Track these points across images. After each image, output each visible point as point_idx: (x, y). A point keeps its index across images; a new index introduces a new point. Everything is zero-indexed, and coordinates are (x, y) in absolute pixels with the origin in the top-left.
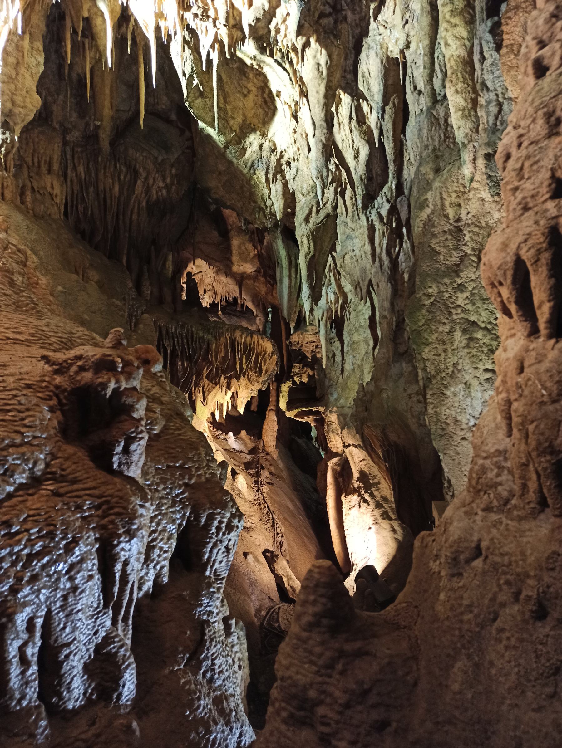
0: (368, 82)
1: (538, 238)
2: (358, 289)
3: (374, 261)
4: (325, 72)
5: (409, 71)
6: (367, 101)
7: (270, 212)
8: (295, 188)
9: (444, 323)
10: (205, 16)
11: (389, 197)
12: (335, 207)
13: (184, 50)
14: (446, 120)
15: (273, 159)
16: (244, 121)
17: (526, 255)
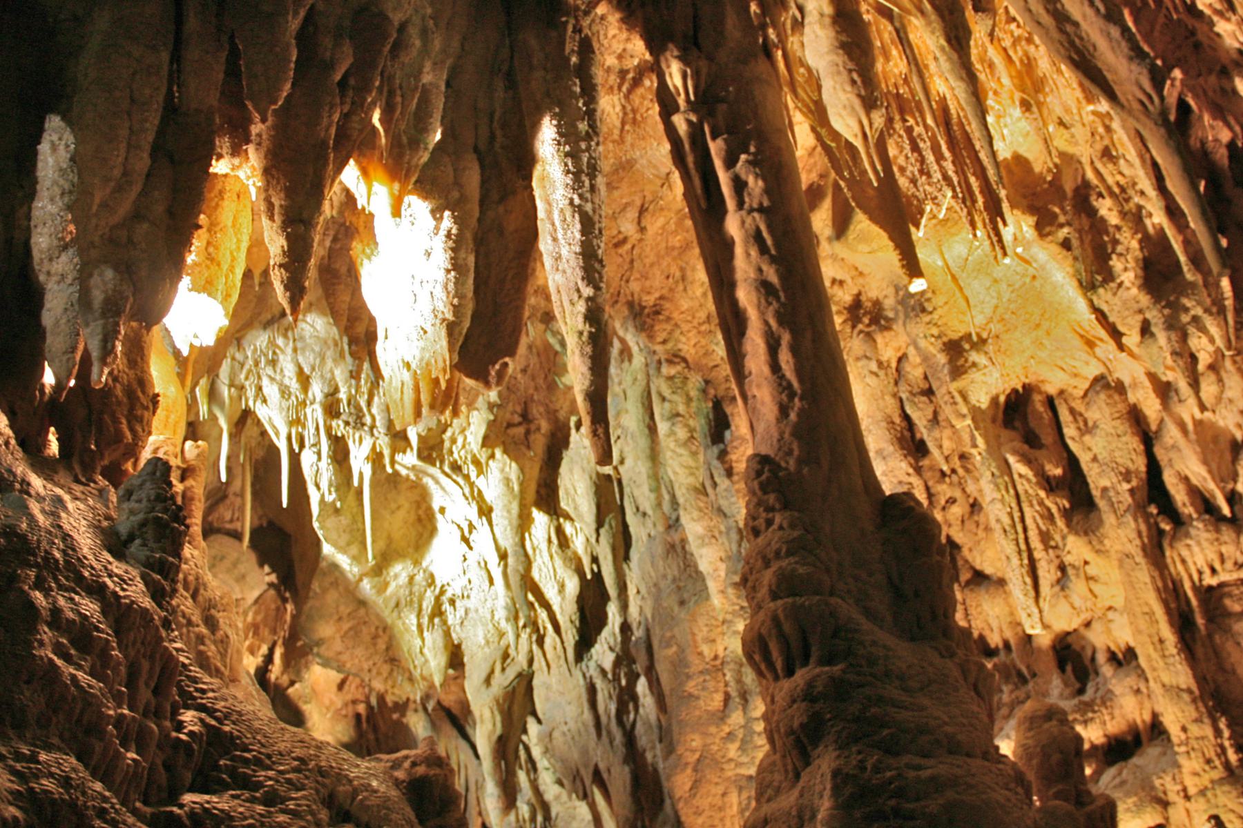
0: (574, 500)
1: (768, 623)
2: (578, 783)
3: (599, 735)
4: (516, 488)
5: (627, 490)
6: (572, 520)
7: (421, 675)
8: (463, 636)
9: (717, 784)
10: (359, 423)
11: (612, 643)
12: (531, 662)
14: (683, 548)
15: (429, 598)
16: (388, 546)
17: (763, 631)
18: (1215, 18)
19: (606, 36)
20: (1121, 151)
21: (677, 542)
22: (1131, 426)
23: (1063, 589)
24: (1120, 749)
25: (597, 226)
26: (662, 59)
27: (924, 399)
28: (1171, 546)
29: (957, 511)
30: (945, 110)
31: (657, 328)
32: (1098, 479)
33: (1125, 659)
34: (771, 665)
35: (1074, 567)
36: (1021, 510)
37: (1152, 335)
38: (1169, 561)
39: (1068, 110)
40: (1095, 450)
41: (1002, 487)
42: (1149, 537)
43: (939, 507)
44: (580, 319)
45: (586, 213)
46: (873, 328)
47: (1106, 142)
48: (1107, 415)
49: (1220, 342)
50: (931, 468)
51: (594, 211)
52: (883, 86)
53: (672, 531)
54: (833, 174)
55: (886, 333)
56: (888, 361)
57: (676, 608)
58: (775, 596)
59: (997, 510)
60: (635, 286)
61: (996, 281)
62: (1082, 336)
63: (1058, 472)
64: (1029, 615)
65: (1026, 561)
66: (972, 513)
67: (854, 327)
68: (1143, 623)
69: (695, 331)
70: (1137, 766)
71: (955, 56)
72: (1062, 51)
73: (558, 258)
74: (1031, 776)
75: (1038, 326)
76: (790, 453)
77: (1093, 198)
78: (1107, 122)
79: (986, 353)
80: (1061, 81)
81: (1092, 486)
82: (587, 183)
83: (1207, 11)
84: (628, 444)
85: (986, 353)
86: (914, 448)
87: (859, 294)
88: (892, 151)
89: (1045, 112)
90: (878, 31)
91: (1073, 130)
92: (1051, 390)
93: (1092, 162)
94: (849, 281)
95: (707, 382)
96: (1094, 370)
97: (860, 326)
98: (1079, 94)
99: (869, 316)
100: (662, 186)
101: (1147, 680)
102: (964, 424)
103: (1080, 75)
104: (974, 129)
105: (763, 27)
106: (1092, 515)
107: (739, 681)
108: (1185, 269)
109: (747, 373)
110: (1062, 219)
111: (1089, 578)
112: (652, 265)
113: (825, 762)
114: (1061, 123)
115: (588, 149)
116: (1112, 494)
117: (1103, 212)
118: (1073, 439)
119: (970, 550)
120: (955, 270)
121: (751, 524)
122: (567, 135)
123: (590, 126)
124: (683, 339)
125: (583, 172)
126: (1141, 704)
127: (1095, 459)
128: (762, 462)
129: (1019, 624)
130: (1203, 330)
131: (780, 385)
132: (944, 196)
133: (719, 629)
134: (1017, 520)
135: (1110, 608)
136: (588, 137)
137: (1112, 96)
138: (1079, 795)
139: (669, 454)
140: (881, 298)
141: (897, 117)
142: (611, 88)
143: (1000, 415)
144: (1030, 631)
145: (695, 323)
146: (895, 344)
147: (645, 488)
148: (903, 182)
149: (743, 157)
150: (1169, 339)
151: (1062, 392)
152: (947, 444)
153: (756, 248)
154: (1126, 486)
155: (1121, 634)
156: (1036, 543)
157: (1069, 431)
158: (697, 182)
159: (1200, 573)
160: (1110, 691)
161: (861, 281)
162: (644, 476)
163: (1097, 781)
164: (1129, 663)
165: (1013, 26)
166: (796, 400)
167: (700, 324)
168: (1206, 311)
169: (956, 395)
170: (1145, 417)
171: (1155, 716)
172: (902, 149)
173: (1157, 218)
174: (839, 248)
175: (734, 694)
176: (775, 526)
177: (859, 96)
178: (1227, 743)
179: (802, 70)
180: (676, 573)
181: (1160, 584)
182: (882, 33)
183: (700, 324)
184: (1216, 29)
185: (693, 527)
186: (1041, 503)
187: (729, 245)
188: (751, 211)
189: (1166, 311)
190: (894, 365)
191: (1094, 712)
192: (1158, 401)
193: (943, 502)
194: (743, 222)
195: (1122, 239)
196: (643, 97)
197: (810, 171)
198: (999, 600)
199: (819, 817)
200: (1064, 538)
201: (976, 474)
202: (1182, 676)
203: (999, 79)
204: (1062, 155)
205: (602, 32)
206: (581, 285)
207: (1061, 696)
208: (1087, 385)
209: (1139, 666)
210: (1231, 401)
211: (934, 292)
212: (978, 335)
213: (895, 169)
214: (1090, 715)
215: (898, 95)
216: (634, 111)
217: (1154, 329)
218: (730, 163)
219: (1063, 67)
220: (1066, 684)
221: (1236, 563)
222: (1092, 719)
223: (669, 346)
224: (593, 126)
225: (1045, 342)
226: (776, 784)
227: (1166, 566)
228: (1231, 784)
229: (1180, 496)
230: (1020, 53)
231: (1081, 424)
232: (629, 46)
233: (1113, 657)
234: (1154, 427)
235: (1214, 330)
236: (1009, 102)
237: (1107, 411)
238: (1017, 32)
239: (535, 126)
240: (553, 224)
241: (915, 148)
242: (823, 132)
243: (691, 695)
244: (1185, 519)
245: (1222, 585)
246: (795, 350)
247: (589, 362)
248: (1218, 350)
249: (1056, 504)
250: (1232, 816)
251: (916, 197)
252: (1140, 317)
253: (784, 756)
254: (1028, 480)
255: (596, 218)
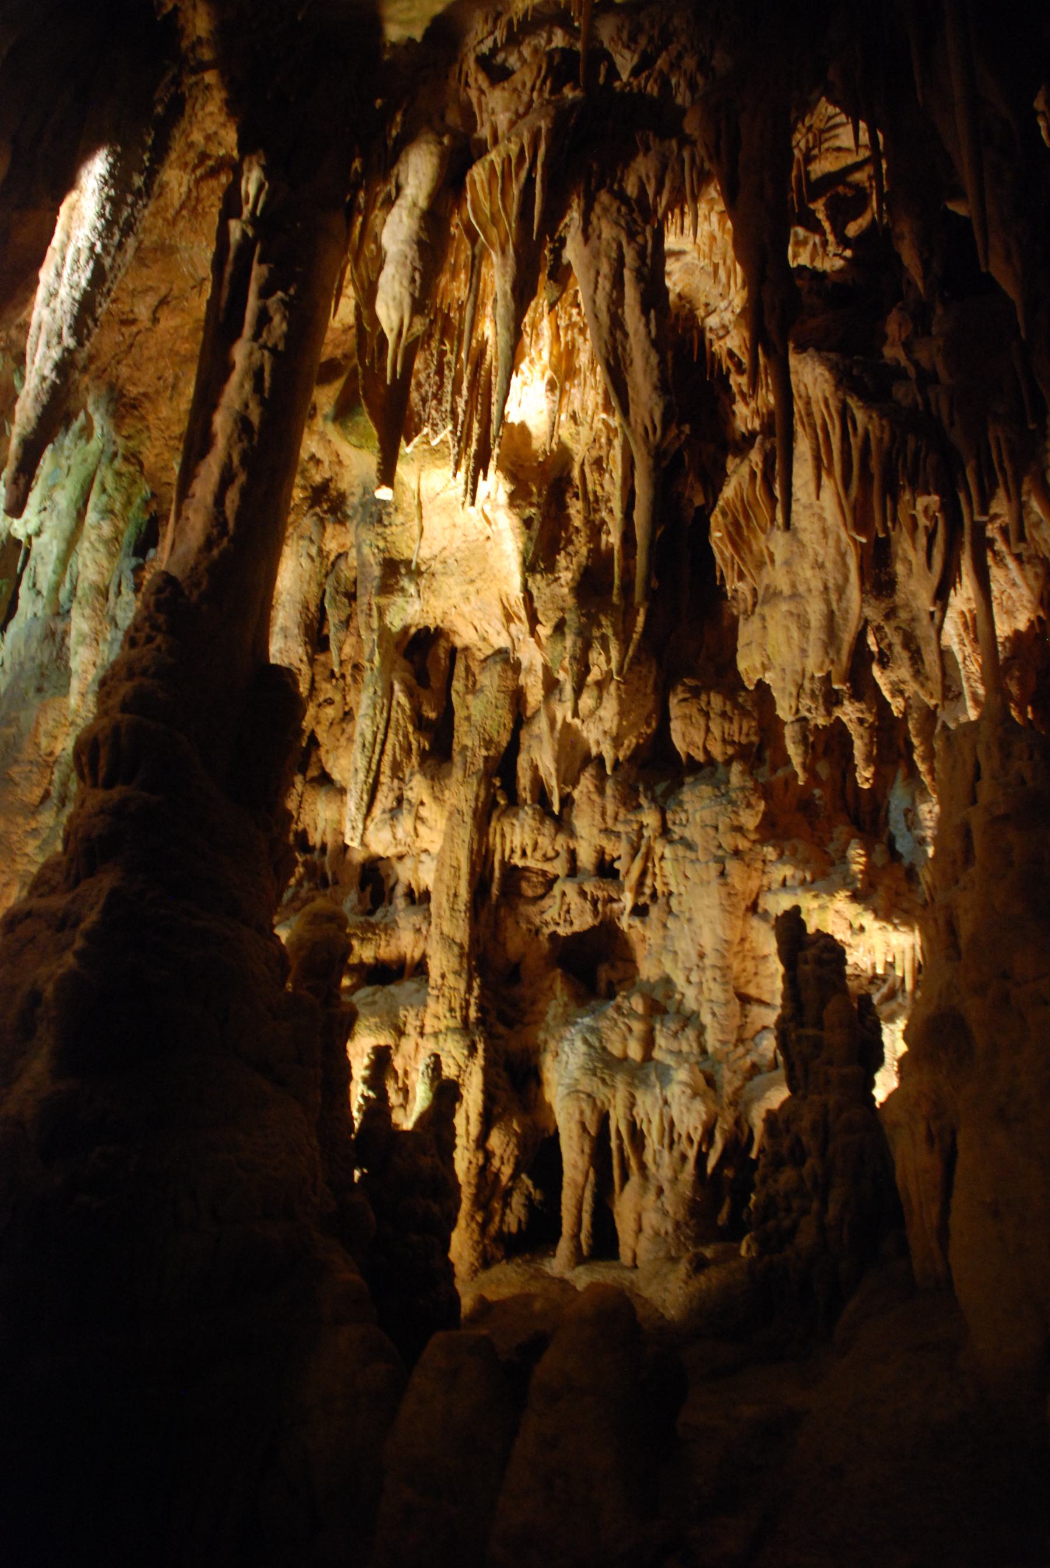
5: (31, 563)
13: (819, 487)
14: (63, 639)
18: (738, 398)
19: (203, 108)
20: (611, 466)
21: (59, 631)
22: (511, 704)
23: (392, 819)
24: (387, 973)
25: (108, 284)
26: (247, 160)
27: (346, 601)
28: (499, 820)
29: (330, 712)
30: (482, 353)
31: (127, 421)
32: (465, 737)
33: (418, 899)
34: (94, 773)
35: (410, 802)
36: (386, 735)
37: (563, 634)
38: (491, 830)
39: (584, 409)
40: (473, 711)
41: (378, 707)
42: (484, 804)
43: (316, 702)
44: (50, 365)
45: (103, 266)
46: (329, 516)
47: (603, 453)
48: (495, 686)
49: (614, 665)
50: (324, 665)
51: (112, 268)
52: (438, 301)
53: (58, 620)
54: (356, 361)
55: (337, 527)
56: (329, 553)
57: (32, 693)
58: (125, 708)
59: (364, 725)
60: (124, 371)
61: (454, 525)
62: (504, 607)
63: (432, 715)
64: (353, 828)
65: (370, 780)
66: (343, 720)
67: (311, 507)
68: (447, 875)
69: (162, 442)
70: (393, 995)
71: (512, 306)
72: (604, 351)
73: (53, 295)
74: (294, 964)
75: (472, 581)
76: (198, 584)
77: (569, 495)
78: (612, 436)
79: (417, 584)
80: (591, 380)
81: (456, 740)
82: (117, 237)
83: (735, 389)
84: (51, 519)
85: (417, 584)
86: (316, 638)
87: (330, 480)
88: (418, 364)
89: (565, 401)
90: (458, 249)
91: (580, 428)
92: (459, 643)
93: (583, 464)
94: (326, 464)
95: (153, 495)
96: (501, 641)
97: (318, 509)
98: (600, 400)
99: (329, 503)
100: (193, 288)
101: (430, 924)
102: (371, 638)
103: (608, 380)
104: (497, 382)
105: (356, 188)
106: (444, 766)
107: (64, 784)
108: (615, 591)
109: (190, 493)
110: (535, 499)
111: (418, 818)
112: (150, 359)
113: (107, 881)
114: (574, 417)
115: (133, 205)
116: (469, 754)
117: (572, 511)
118: (458, 693)
119: (327, 752)
120: (423, 499)
121: (132, 633)
122: (117, 179)
123: (145, 183)
124: (148, 444)
125: (117, 222)
126: (417, 942)
127: (468, 718)
128: (167, 580)
129: (342, 834)
130: (606, 649)
131: (216, 518)
132: (444, 427)
133: (65, 729)
134: (378, 740)
135: (426, 851)
136: (138, 194)
137: (625, 412)
138: (331, 995)
139: (86, 544)
140: (348, 492)
141: (437, 337)
142: (186, 164)
143: (405, 643)
144: (348, 842)
145: (167, 434)
146: (341, 540)
147: (50, 568)
148: (415, 396)
149: (280, 294)
150: (575, 644)
151: (466, 649)
152: (347, 650)
153: (252, 383)
154: (484, 753)
155: (426, 876)
156: (386, 768)
157: (458, 685)
158: (225, 294)
159: (512, 851)
160: (396, 922)
161: (337, 468)
162: (54, 557)
163: (353, 994)
164: (421, 903)
165: (575, 311)
166: (225, 540)
167: (171, 438)
168: (615, 634)
169: (374, 608)
170: (526, 701)
171: (424, 956)
172: (427, 366)
173: (613, 538)
174: (332, 431)
175: (54, 793)
176: (153, 646)
177: (412, 295)
178: (473, 1001)
179: (373, 246)
180: (46, 661)
181: (475, 847)
182: (461, 253)
183: (171, 438)
184: (734, 407)
185: (80, 623)
186: (406, 736)
187: (228, 367)
188: (264, 347)
189: (583, 620)
190: (332, 558)
191: (375, 934)
192: (542, 692)
193: (321, 699)
194: (251, 354)
195: (576, 542)
196: (213, 191)
197: (337, 346)
198: (334, 807)
199: (82, 926)
200: (412, 774)
201: (361, 686)
202: (461, 933)
203: (540, 350)
204: (560, 443)
205: (200, 101)
206: (65, 331)
207: (352, 909)
208: (490, 652)
209: (428, 910)
210: (601, 719)
211: (396, 509)
212: (418, 565)
213: (413, 382)
214: (370, 935)
215: (447, 317)
216: (198, 200)
217: (566, 630)
218: (265, 293)
219: (599, 369)
220: (360, 901)
221: (544, 855)
222: (370, 939)
223: (131, 444)
224: (149, 184)
225: (472, 598)
226: (53, 883)
227: (487, 834)
228: (462, 1035)
229: (524, 780)
230: (569, 338)
231: (470, 683)
232: (222, 132)
233: (410, 893)
234: (529, 713)
235: (614, 654)
236: (540, 375)
237: (496, 681)
238: (575, 318)
239: (86, 154)
240: (64, 259)
241: (440, 372)
242: (365, 313)
243: (12, 780)
244: (520, 802)
245: (526, 869)
246: (244, 493)
247: (39, 410)
248: (609, 672)
249: (419, 742)
250: (451, 1062)
251: (420, 416)
252: (560, 614)
253: (71, 860)
254: (404, 711)
255: (110, 277)
